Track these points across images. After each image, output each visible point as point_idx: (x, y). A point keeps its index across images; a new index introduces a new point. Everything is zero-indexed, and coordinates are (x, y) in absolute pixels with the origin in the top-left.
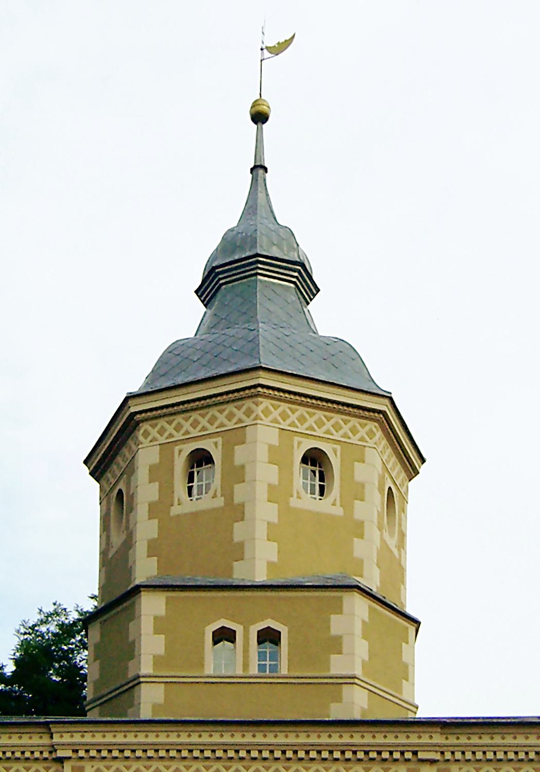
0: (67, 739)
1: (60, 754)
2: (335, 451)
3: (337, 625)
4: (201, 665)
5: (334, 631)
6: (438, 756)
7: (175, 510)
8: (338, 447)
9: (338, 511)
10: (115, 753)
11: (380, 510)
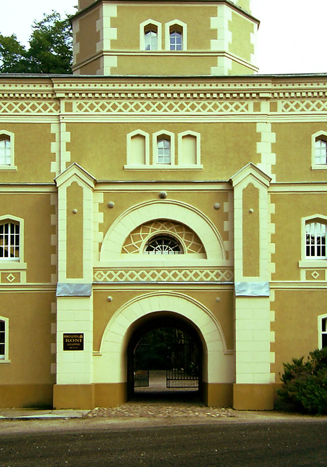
0: (62, 87)
1: (58, 95)
3: (214, 23)
4: (175, 50)
5: (213, 26)
6: (270, 95)
10: (202, 95)
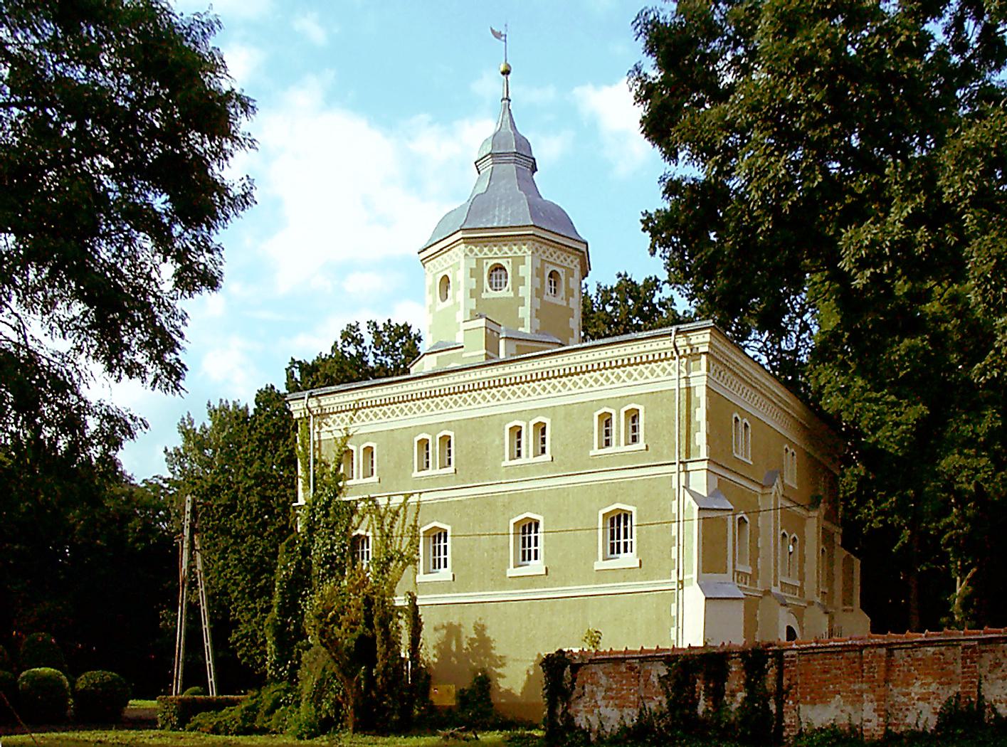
2: (508, 262)
7: (484, 296)
8: (510, 260)
9: (511, 294)
11: (539, 287)
